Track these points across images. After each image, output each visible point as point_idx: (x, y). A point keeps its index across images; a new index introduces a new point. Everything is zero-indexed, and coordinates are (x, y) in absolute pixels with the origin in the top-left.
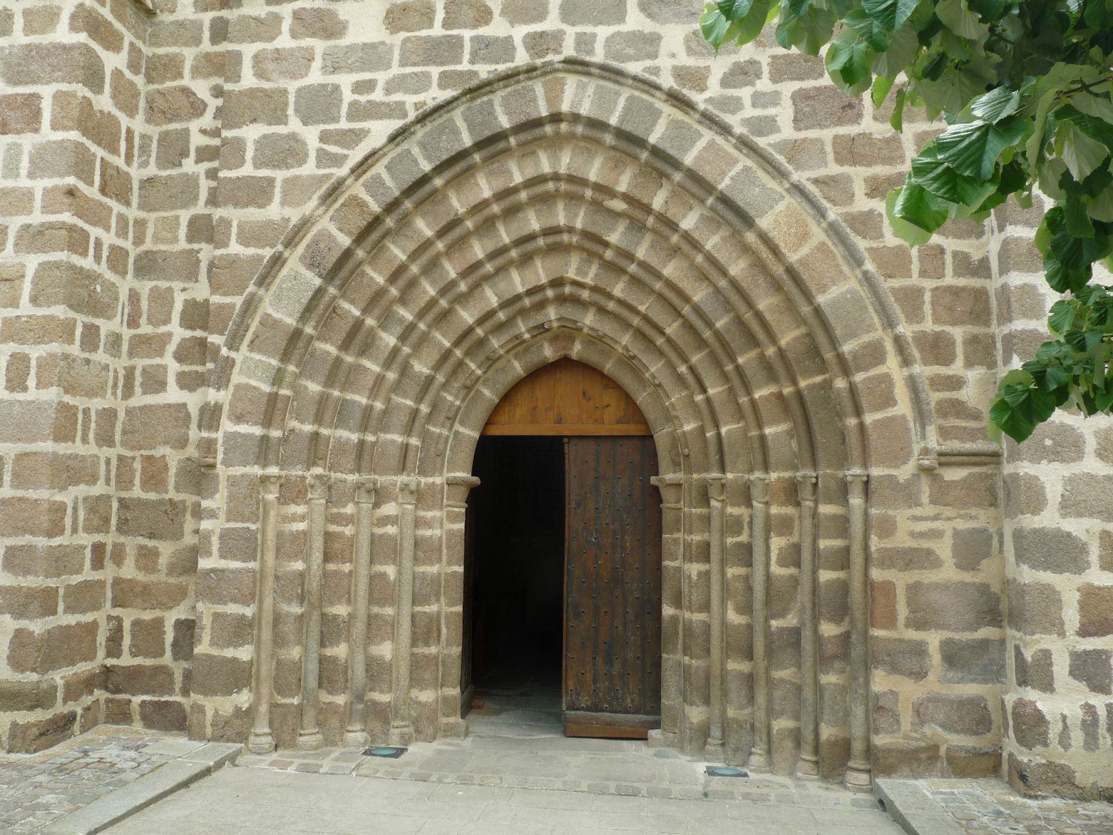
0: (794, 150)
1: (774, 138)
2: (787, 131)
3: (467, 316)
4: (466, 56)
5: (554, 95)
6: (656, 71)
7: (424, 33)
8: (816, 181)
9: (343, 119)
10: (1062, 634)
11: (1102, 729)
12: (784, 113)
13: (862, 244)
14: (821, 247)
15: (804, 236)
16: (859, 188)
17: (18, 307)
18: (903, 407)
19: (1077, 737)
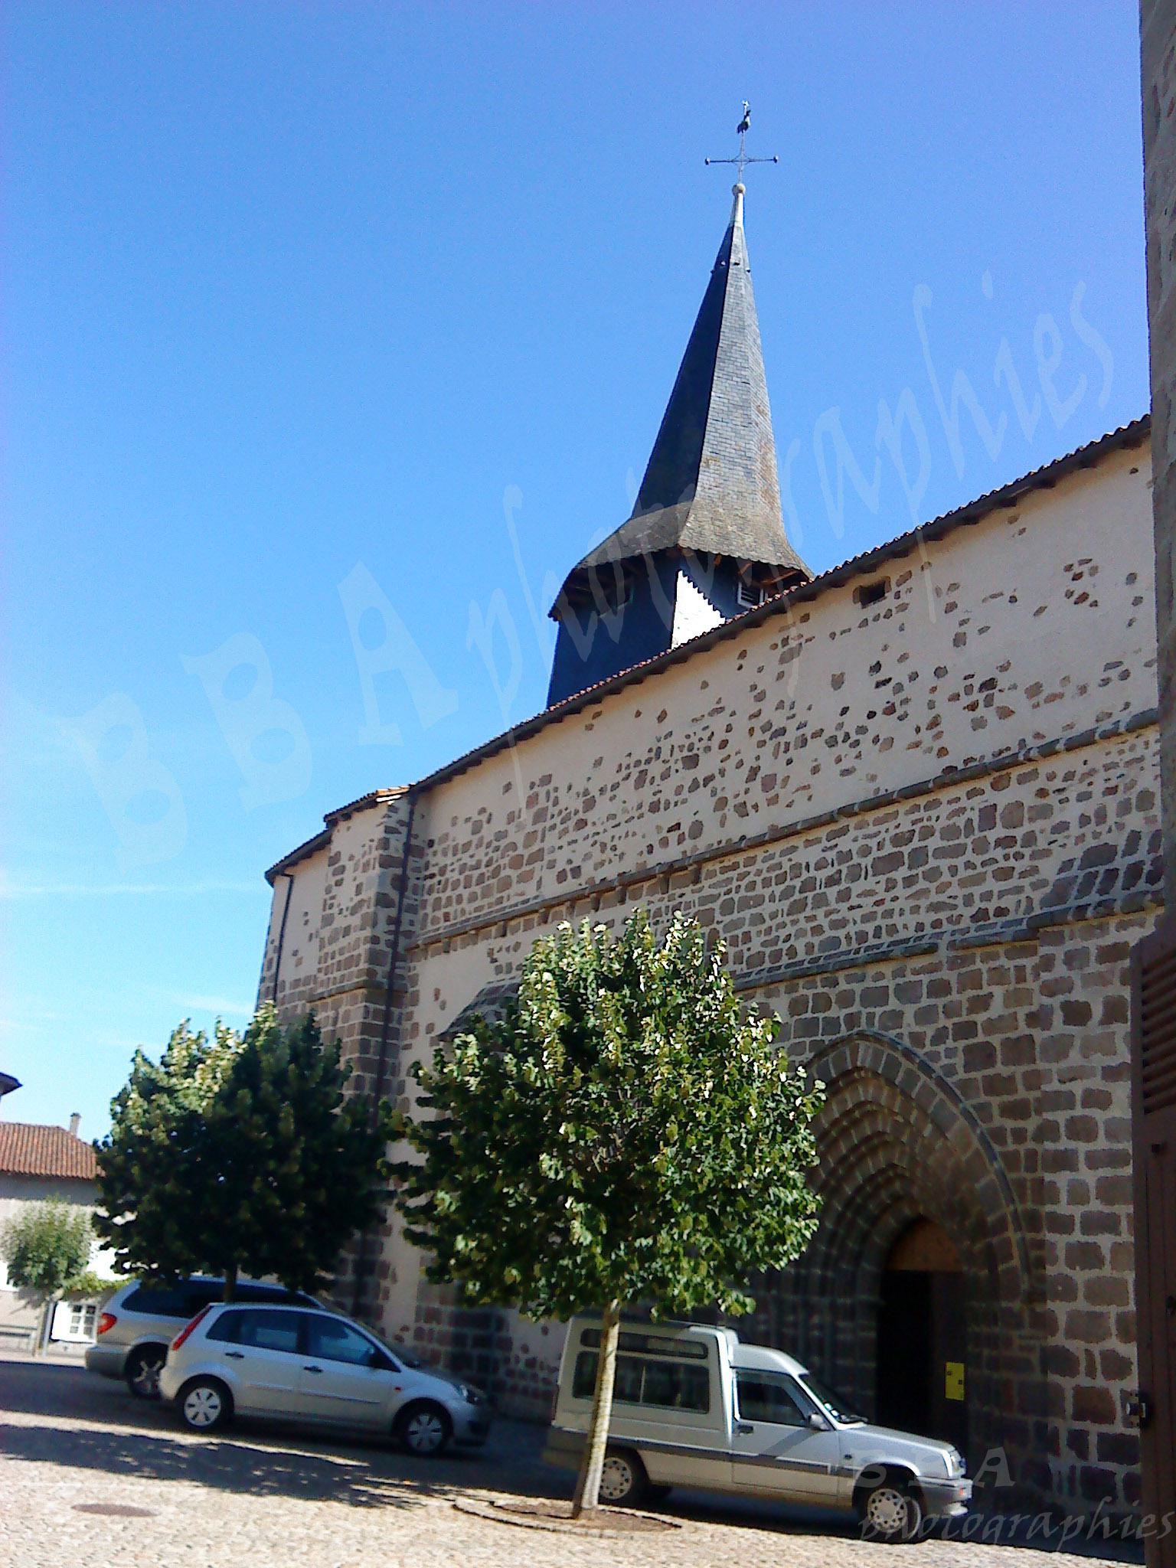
0: (965, 1085)
1: (955, 1078)
2: (961, 1075)
3: (848, 1190)
4: (843, 1027)
5: (855, 1051)
6: (900, 1036)
7: (803, 1016)
8: (974, 1107)
9: (1064, 1138)
10: (1064, 1418)
11: (1078, 1484)
12: (959, 1061)
13: (997, 1148)
14: (977, 1152)
15: (968, 1145)
16: (996, 1111)
17: (550, 615)
18: (1016, 1262)
19: (1066, 1486)
